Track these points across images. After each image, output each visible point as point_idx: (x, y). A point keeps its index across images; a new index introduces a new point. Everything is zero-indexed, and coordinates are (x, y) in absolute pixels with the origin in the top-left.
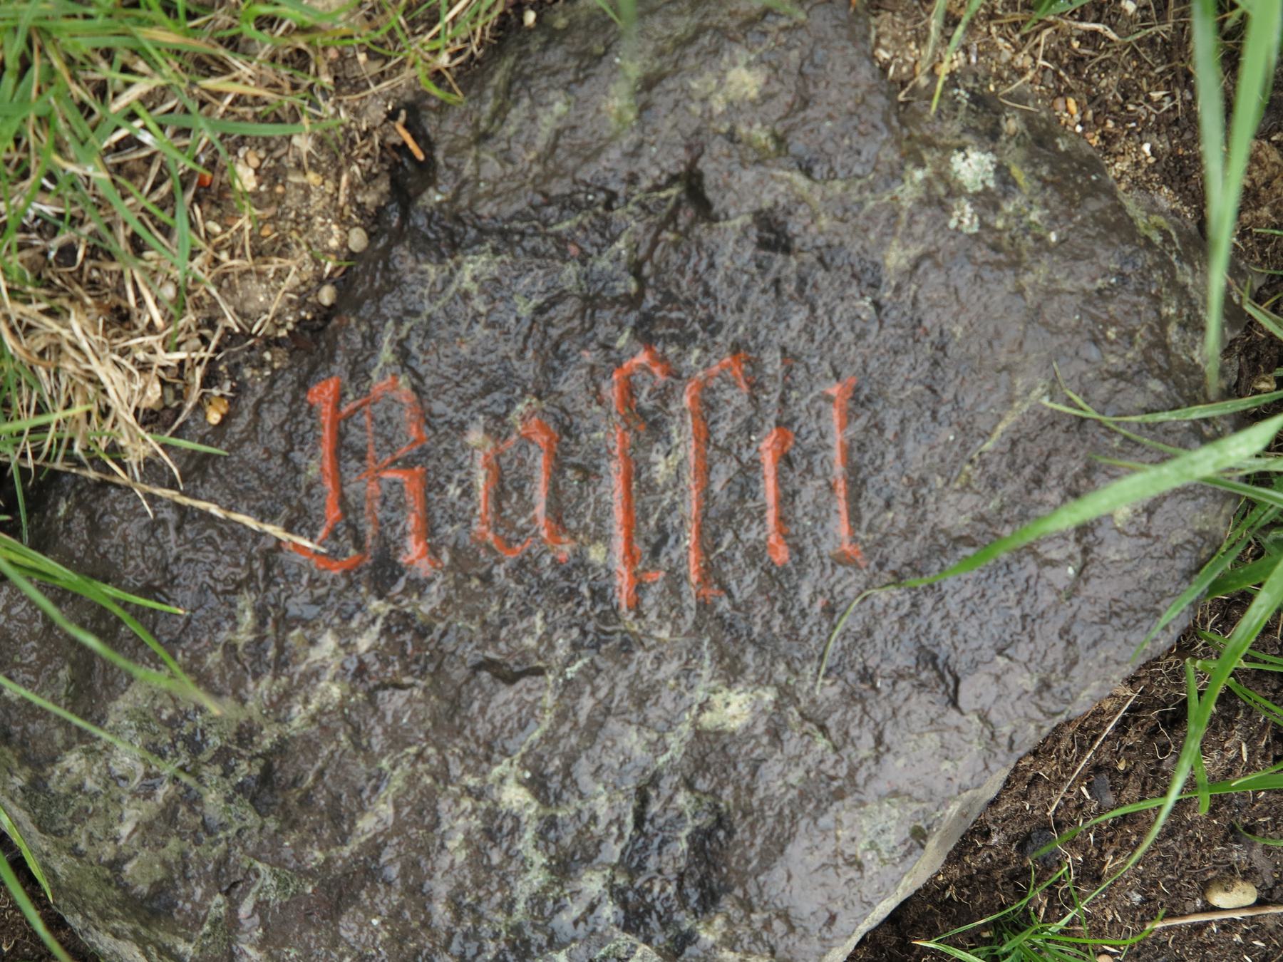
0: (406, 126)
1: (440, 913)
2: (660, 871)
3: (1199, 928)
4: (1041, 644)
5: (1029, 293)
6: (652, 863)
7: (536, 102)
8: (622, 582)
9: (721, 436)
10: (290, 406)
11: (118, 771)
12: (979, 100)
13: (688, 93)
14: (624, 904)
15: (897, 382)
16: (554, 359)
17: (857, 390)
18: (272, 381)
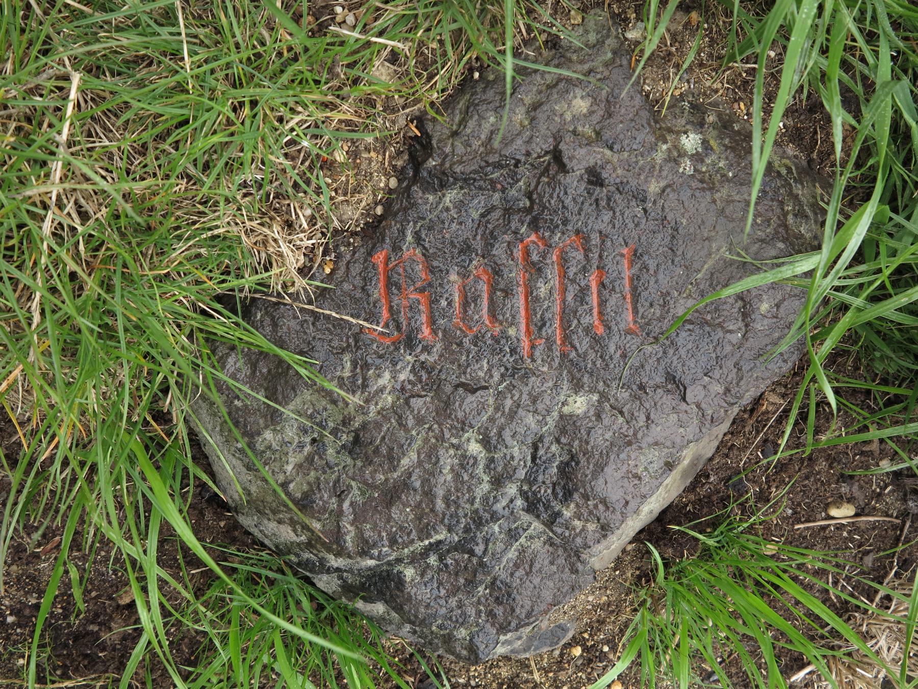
0: (416, 127)
1: (440, 505)
2: (544, 483)
3: (824, 528)
4: (725, 370)
5: (718, 202)
6: (540, 478)
7: (481, 117)
8: (525, 344)
9: (571, 274)
11: (287, 439)
12: (694, 107)
13: (554, 112)
14: (527, 499)
15: (655, 246)
16: (490, 239)
17: (636, 251)
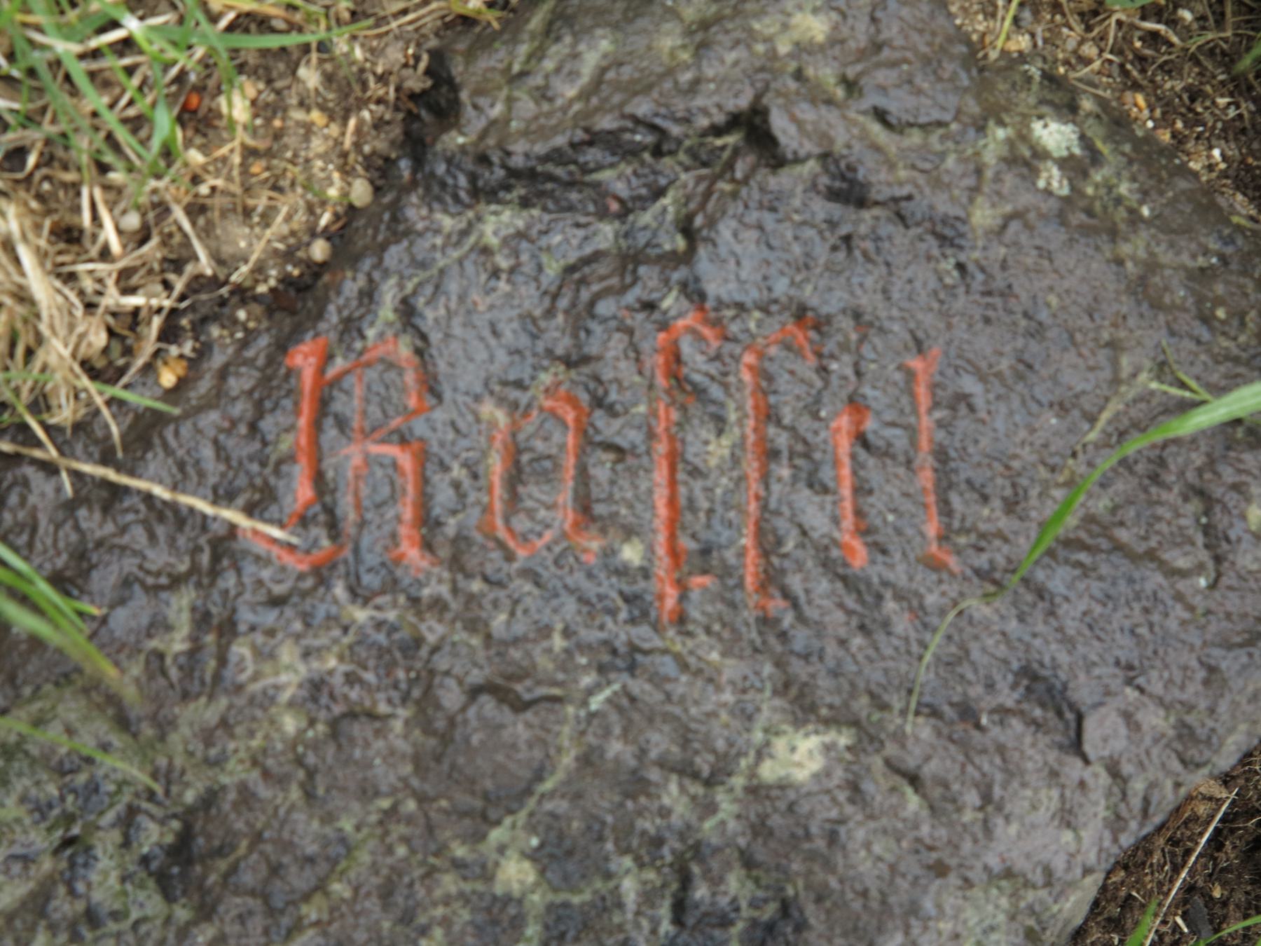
10: (262, 370)
18: (244, 344)
